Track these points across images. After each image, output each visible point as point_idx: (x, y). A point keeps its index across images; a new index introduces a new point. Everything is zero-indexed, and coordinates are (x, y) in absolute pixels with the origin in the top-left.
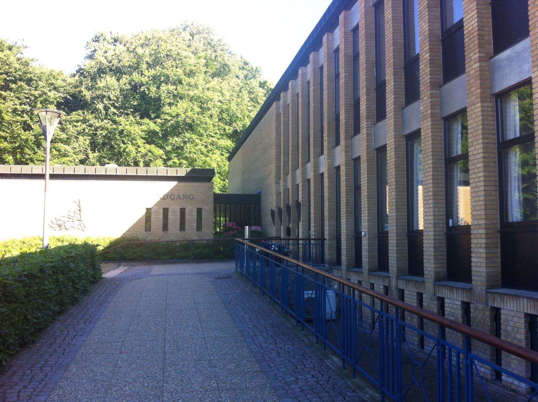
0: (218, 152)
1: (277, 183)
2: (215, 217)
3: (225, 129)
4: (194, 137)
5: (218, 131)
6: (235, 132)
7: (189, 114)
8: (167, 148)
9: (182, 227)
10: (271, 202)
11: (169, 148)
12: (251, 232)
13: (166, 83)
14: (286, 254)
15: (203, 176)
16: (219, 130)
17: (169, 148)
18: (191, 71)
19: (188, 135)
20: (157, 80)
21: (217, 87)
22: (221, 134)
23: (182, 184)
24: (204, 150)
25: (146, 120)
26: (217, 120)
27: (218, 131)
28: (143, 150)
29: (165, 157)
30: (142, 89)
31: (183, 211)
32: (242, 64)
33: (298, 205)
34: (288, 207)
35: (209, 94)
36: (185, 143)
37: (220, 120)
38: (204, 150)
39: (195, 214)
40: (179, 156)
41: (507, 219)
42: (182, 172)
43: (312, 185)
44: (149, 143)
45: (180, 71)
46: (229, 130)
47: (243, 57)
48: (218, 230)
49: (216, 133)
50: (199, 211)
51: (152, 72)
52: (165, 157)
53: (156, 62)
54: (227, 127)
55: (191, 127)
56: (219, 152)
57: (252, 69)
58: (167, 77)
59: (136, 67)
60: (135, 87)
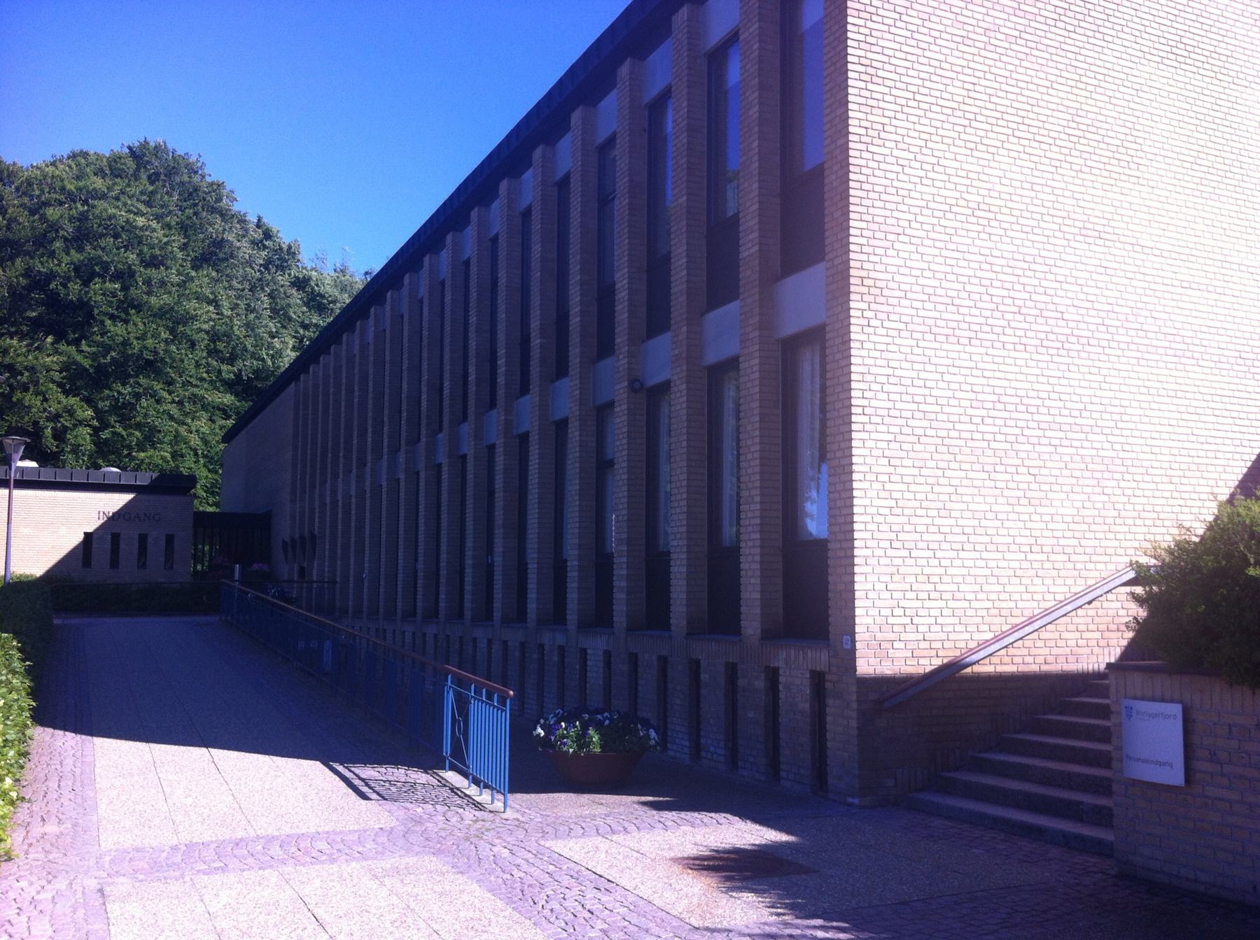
0: (205, 415)
1: (293, 501)
2: (195, 545)
3: (220, 372)
4: (158, 386)
5: (205, 375)
6: (238, 375)
7: (150, 342)
8: (101, 404)
9: (114, 563)
10: (284, 529)
11: (104, 405)
12: (242, 573)
13: (102, 277)
14: (289, 601)
15: (173, 484)
16: (207, 372)
17: (104, 405)
18: (154, 257)
19: (143, 381)
20: (85, 273)
21: (207, 292)
22: (211, 382)
23: (143, 497)
24: (174, 410)
25: (63, 347)
26: (205, 354)
27: (205, 375)
28: (53, 408)
29: (96, 423)
30: (52, 286)
31: (143, 539)
32: (258, 235)
33: (313, 537)
34: (302, 537)
35: (191, 305)
36: (138, 396)
37: (210, 353)
38: (174, 410)
39: (163, 543)
40: (123, 420)
41: (813, 588)
42: (144, 479)
43: (445, 476)
44: (66, 393)
45: (132, 257)
46: (227, 371)
47: (265, 220)
48: (199, 567)
49: (202, 379)
50: (170, 539)
51: (76, 256)
52: (96, 423)
53: (81, 237)
54: (224, 367)
55: (151, 366)
56: (205, 415)
57: (281, 249)
58: (105, 266)
59: (42, 242)
60: (39, 282)
